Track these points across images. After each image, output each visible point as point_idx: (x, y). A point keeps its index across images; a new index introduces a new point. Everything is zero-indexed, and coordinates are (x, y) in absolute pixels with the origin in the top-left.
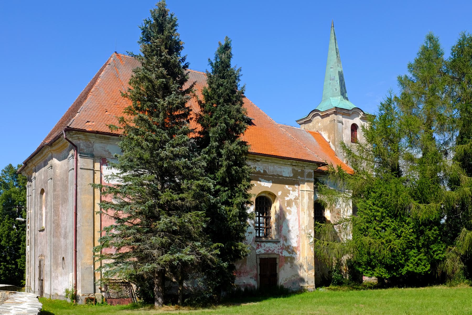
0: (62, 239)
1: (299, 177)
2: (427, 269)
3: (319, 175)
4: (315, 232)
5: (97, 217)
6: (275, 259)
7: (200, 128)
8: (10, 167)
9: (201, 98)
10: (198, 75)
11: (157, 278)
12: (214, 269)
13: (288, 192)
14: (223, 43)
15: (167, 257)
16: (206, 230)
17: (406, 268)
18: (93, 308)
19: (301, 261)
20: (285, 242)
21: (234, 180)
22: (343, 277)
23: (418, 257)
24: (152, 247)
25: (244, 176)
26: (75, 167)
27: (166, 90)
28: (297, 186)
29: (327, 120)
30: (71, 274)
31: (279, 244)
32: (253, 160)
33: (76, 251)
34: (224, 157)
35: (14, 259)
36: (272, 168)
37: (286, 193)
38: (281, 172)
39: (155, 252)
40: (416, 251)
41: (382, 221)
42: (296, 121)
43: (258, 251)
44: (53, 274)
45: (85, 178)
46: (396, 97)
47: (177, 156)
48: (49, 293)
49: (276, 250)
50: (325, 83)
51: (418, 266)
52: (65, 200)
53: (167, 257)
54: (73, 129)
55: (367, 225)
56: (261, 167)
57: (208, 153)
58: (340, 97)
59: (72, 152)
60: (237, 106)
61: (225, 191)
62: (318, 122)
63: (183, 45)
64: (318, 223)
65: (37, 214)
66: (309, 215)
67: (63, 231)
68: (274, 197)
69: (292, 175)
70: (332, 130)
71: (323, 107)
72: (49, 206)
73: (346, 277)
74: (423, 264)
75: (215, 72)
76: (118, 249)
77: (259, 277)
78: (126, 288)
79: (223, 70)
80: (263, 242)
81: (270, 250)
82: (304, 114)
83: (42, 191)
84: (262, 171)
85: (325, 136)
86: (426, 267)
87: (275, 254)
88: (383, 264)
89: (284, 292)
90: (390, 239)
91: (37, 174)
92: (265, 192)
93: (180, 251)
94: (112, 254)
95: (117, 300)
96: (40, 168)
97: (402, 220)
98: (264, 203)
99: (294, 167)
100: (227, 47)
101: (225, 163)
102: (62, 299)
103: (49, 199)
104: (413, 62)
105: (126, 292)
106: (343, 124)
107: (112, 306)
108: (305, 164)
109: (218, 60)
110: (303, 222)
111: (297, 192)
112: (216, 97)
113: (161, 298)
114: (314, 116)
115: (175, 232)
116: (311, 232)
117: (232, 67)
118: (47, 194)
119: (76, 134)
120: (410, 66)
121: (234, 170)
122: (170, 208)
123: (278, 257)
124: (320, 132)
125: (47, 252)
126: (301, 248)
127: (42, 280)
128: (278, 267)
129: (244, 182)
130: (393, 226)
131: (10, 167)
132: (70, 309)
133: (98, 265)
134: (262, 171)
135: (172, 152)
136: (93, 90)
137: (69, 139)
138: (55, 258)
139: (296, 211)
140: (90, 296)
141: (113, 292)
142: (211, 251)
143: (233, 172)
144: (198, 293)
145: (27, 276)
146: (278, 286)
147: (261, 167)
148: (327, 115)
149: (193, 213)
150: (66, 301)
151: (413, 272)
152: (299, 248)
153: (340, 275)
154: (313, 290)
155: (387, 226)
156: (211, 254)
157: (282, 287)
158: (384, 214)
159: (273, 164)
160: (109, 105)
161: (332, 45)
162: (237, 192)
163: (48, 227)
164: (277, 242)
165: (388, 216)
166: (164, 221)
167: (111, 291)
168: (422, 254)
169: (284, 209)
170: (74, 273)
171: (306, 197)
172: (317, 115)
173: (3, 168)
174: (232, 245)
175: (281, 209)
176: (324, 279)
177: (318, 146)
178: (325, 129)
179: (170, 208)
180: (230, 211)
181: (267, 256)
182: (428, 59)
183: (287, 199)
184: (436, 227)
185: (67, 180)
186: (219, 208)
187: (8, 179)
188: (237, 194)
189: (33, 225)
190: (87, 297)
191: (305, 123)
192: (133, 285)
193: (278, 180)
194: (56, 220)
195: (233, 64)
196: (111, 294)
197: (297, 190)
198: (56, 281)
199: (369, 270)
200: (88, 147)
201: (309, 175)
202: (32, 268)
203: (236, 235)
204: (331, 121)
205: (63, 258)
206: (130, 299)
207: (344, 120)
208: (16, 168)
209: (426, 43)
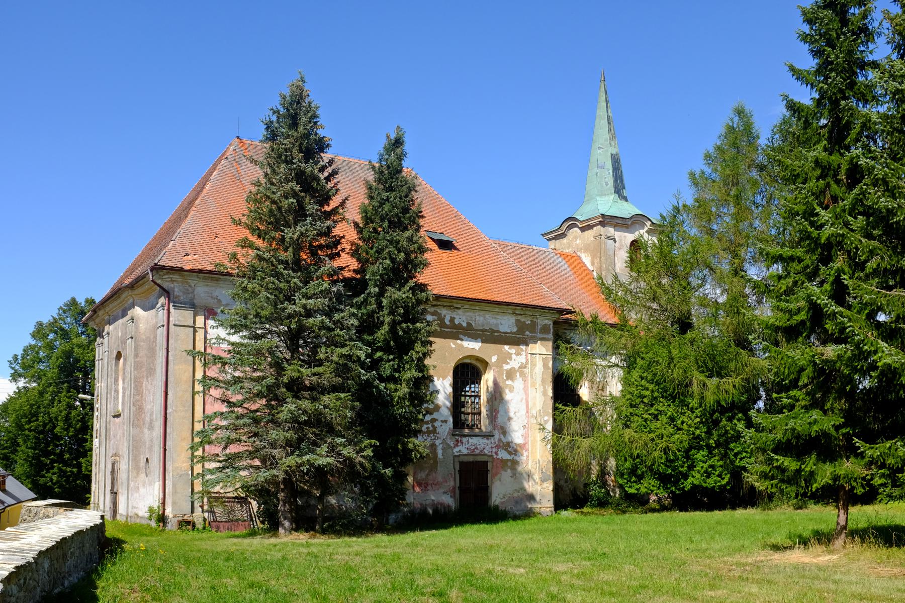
0: (146, 431)
1: (527, 333)
2: (724, 482)
3: (562, 328)
4: (554, 420)
5: (199, 399)
6: (486, 463)
7: (354, 264)
8: (74, 302)
9: (358, 218)
10: (352, 192)
11: (283, 490)
13: (509, 356)
14: (393, 136)
15: (292, 460)
17: (690, 480)
18: (188, 535)
19: (530, 467)
20: (502, 437)
21: (403, 345)
22: (609, 494)
23: (710, 462)
24: (273, 445)
25: (417, 338)
27: (300, 213)
28: (523, 347)
29: (590, 234)
30: (157, 483)
31: (492, 440)
32: (450, 306)
33: (165, 450)
34: (386, 311)
35: (77, 458)
36: (482, 319)
37: (506, 358)
38: (497, 325)
40: (705, 453)
41: (652, 405)
42: (543, 235)
43: (456, 450)
44: (132, 484)
45: (181, 340)
46: (685, 206)
47: (309, 313)
48: (125, 513)
49: (487, 448)
50: (589, 174)
51: (708, 477)
52: (151, 372)
53: (292, 460)
54: (164, 268)
55: (631, 410)
56: (464, 318)
57: (365, 302)
58: (613, 197)
59: (162, 300)
60: (408, 233)
61: (389, 361)
62: (576, 238)
63: (330, 142)
64: (560, 406)
66: (545, 393)
67: (148, 419)
68: (486, 364)
69: (515, 330)
70: (597, 250)
71: (582, 215)
72: (127, 380)
73: (615, 493)
74: (717, 473)
75: (378, 181)
76: (225, 448)
77: (457, 492)
78: (242, 506)
79: (391, 179)
80: (465, 436)
81: (476, 448)
83: (119, 356)
84: (465, 325)
85: (587, 259)
86: (723, 479)
87: (485, 455)
88: (655, 473)
89: (496, 516)
90: (666, 434)
91: (112, 327)
92: (464, 358)
93: (313, 452)
94: (217, 455)
95: (227, 524)
96: (116, 319)
97: (683, 404)
98: (467, 373)
99: (519, 317)
100: (398, 142)
101: (387, 319)
102: (144, 522)
103: (128, 368)
104: (712, 150)
105: (240, 512)
106: (615, 241)
107: (219, 533)
109: (384, 163)
110: (534, 404)
111: (524, 356)
112: (378, 220)
113: (289, 521)
114: (570, 227)
118: (125, 360)
119: (167, 274)
120: (708, 157)
121: (402, 329)
122: (296, 387)
123: (490, 459)
124: (579, 253)
125: (124, 451)
126: (530, 446)
127: (116, 493)
128: (489, 476)
129: (418, 346)
130: (669, 414)
131: (74, 302)
132: (152, 536)
133: (198, 469)
134: (465, 325)
135: (304, 307)
136: (197, 202)
137: (157, 281)
138: (136, 459)
139: (522, 386)
140: (185, 518)
141: (220, 514)
142: (362, 450)
143: (401, 333)
144: (345, 515)
145: (94, 487)
146: (490, 507)
147: (464, 318)
148: (590, 227)
150: (149, 525)
151: (700, 486)
152: (527, 446)
153: (603, 491)
154: (550, 514)
155: (660, 412)
156: (362, 457)
157: (496, 507)
158: (656, 394)
159: (482, 313)
160: (217, 234)
161: (601, 111)
162: (407, 363)
163: (126, 411)
164: (488, 436)
165: (663, 397)
166: (290, 406)
167: (218, 510)
168: (717, 458)
169: (501, 384)
170: (161, 482)
171: (539, 368)
172: (574, 226)
173: (61, 304)
174: (398, 442)
175: (496, 383)
176: (571, 494)
178: (587, 249)
179: (296, 387)
180: (396, 390)
181: (471, 459)
182: (735, 145)
183: (506, 367)
184: (740, 415)
185: (155, 342)
186: (377, 387)
187: (68, 323)
188: (407, 366)
189: (104, 407)
190: (180, 519)
191: (556, 238)
192: (252, 501)
194: (138, 401)
195: (409, 168)
196: (218, 515)
197: (524, 353)
198: (136, 495)
199: (634, 482)
200: (186, 292)
201: (545, 329)
202: (102, 474)
203: (405, 427)
204: (595, 237)
205: (147, 460)
206: (247, 523)
207: (617, 235)
208: (83, 305)
209: (732, 120)
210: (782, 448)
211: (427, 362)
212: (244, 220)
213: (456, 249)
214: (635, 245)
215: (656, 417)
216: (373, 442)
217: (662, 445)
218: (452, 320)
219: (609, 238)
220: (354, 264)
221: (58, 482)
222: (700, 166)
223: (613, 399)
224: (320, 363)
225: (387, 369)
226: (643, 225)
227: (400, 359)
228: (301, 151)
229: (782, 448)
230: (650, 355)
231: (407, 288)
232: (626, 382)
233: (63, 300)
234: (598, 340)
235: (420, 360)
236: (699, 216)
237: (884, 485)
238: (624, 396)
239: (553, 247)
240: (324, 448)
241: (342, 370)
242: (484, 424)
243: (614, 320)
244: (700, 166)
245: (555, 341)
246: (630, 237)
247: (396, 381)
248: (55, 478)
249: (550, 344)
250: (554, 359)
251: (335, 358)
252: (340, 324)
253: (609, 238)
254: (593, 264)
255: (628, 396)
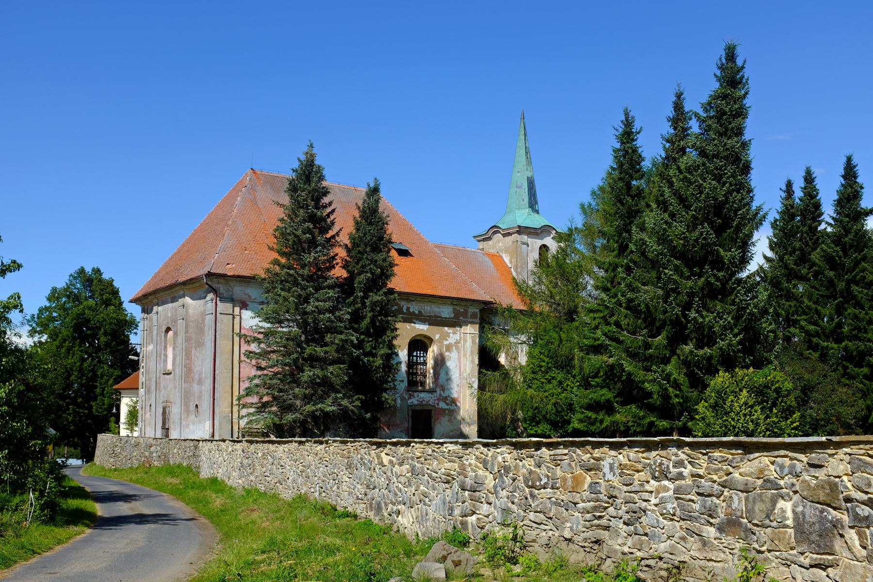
3: (486, 314)
4: (479, 380)
6: (430, 411)
8: (82, 271)
10: (344, 224)
12: (355, 420)
13: (448, 334)
14: (372, 185)
15: (309, 408)
16: (350, 382)
21: (381, 331)
24: (295, 397)
26: (214, 312)
27: (313, 243)
28: (458, 329)
29: (509, 239)
35: (88, 402)
36: (429, 309)
37: (445, 336)
38: (440, 312)
39: (298, 402)
41: (547, 373)
44: (184, 423)
45: (225, 322)
46: (576, 228)
52: (200, 344)
53: (309, 408)
54: (214, 274)
55: (532, 376)
61: (369, 342)
62: (499, 241)
65: (160, 354)
66: (473, 362)
67: (196, 377)
68: (431, 340)
70: (515, 252)
75: (362, 217)
77: (410, 431)
79: (371, 215)
82: (483, 229)
83: (168, 329)
84: (417, 312)
85: (507, 259)
93: (322, 403)
98: (419, 345)
101: (369, 315)
104: (596, 189)
108: (469, 304)
110: (465, 369)
114: (495, 233)
115: (318, 384)
116: (473, 382)
117: (380, 210)
118: (176, 334)
120: (593, 193)
122: (313, 360)
129: (389, 333)
131: (82, 271)
133: (235, 415)
134: (417, 312)
135: (317, 307)
138: (186, 405)
148: (509, 234)
149: (336, 366)
155: (553, 378)
160: (260, 258)
171: (469, 343)
177: (495, 274)
178: (507, 251)
179: (313, 360)
180: (374, 362)
181: (418, 408)
183: (446, 343)
186: (362, 360)
191: (484, 240)
193: (436, 321)
201: (474, 316)
205: (197, 406)
207: (530, 241)
210: (589, 407)
211: (395, 342)
212: (275, 247)
213: (411, 255)
214: (544, 248)
215: (549, 382)
216: (361, 396)
217: (553, 401)
218: (408, 309)
219: (524, 244)
220: (344, 274)
221: (73, 421)
222: (587, 199)
223: (521, 367)
224: (326, 345)
225: (368, 347)
226: (550, 233)
227: (377, 341)
228: (312, 200)
229: (589, 407)
230: (547, 337)
231: (381, 292)
232: (530, 355)
233: (74, 269)
234: (512, 324)
235: (390, 341)
236: (586, 237)
237: (633, 426)
238: (528, 365)
239: (481, 247)
240: (329, 401)
241: (340, 349)
242: (429, 381)
243: (522, 307)
244: (587, 199)
245: (480, 324)
246: (539, 243)
247: (374, 355)
248: (70, 418)
249: (478, 326)
250: (480, 337)
251: (337, 341)
252: (340, 320)
253: (524, 244)
254: (511, 262)
255: (531, 366)
